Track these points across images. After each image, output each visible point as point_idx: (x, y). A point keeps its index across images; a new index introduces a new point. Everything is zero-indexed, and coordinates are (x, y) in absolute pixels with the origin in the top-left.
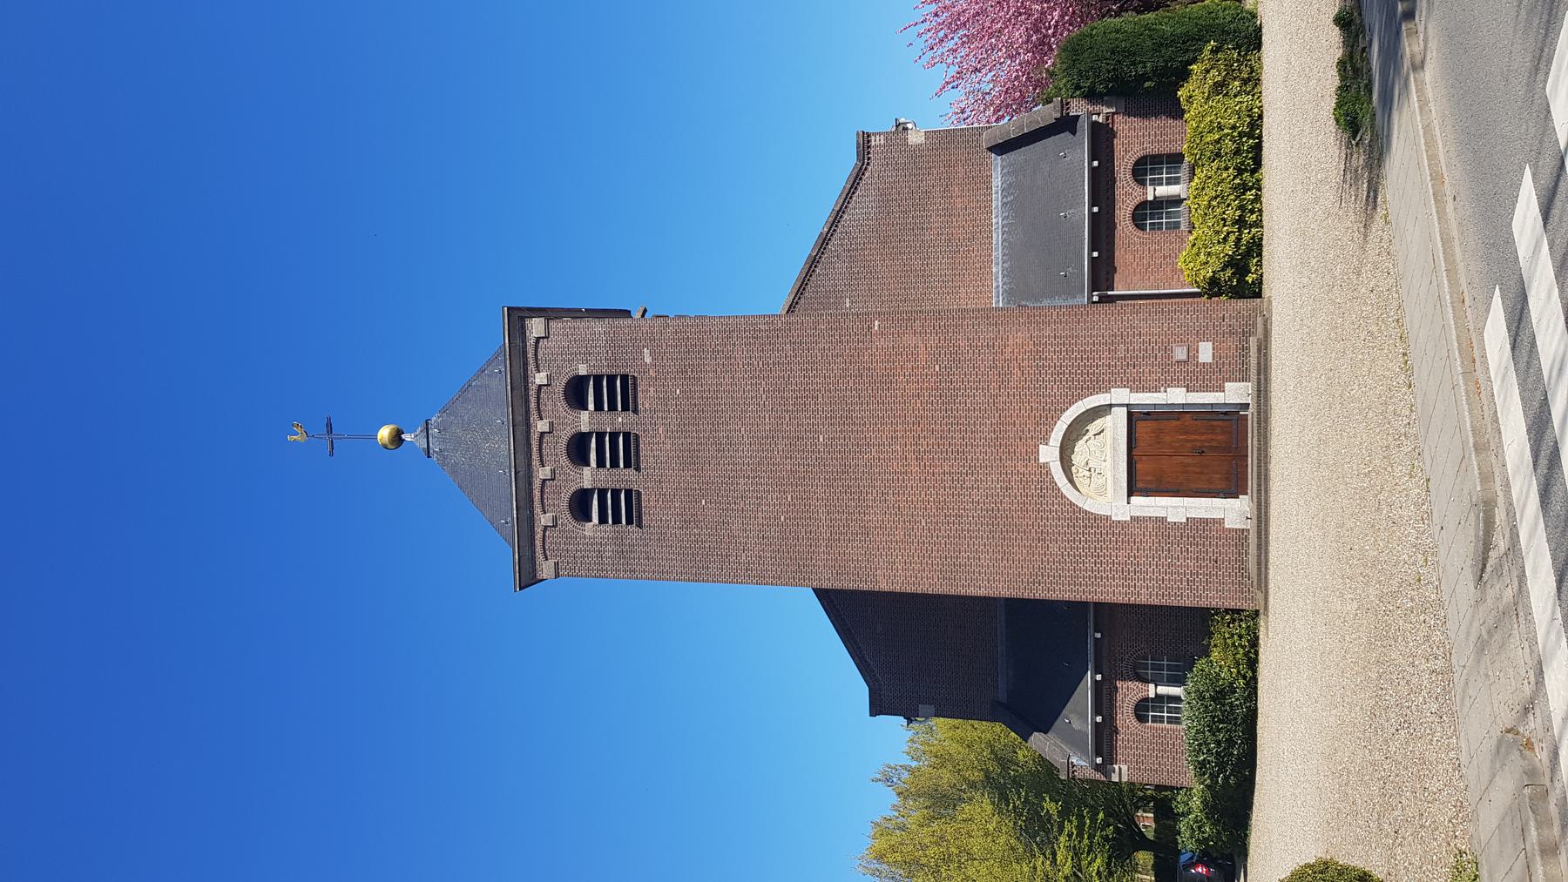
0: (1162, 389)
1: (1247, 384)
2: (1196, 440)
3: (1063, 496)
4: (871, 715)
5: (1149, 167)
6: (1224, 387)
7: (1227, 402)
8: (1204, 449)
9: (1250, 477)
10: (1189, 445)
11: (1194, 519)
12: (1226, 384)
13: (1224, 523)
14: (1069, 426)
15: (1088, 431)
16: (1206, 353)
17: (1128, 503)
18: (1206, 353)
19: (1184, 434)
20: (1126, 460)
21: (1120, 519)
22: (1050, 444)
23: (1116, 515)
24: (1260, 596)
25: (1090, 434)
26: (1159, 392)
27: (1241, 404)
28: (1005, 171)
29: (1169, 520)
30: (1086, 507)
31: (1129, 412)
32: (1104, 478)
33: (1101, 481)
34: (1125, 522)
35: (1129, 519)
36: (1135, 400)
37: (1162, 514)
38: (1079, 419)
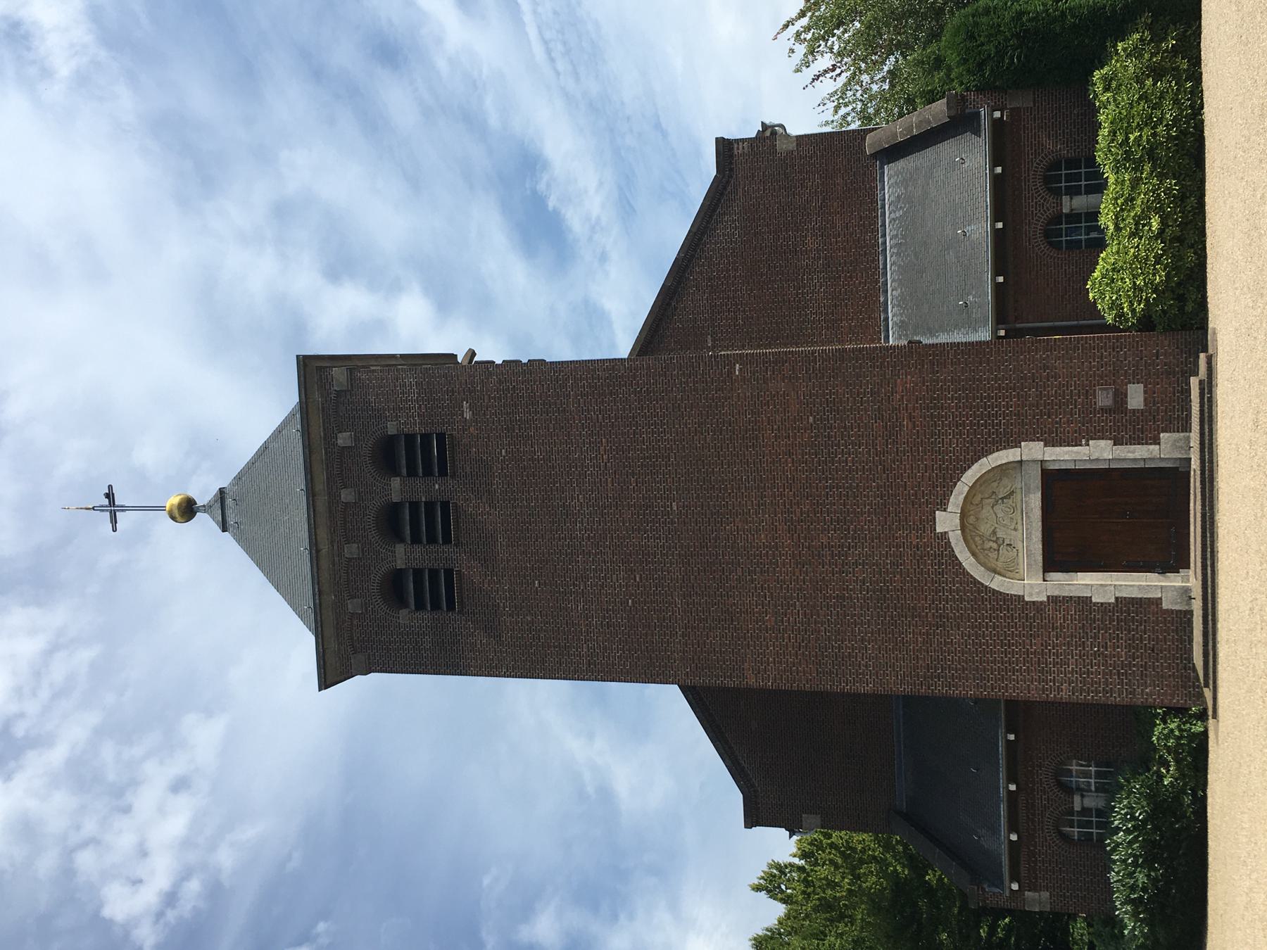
4: (745, 827)
5: (1064, 172)
6: (1159, 439)
9: (1192, 520)
12: (1162, 435)
14: (971, 487)
16: (1136, 397)
18: (1136, 397)
22: (948, 510)
24: (1208, 693)
26: (1081, 445)
27: (1180, 458)
28: (892, 181)
38: (982, 481)
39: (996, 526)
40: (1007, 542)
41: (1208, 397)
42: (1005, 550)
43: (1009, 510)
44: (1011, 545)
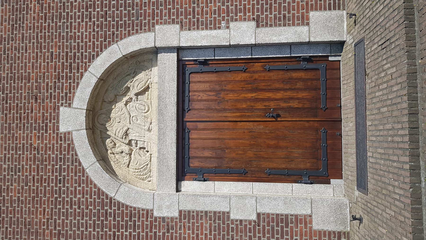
0: (223, 24)
1: (340, 12)
2: (269, 99)
3: (89, 181)
6: (308, 19)
7: (312, 40)
8: (280, 112)
10: (260, 106)
11: (268, 214)
13: (311, 222)
15: (128, 89)
17: (178, 190)
19: (253, 90)
20: (175, 128)
21: (165, 215)
23: (160, 208)
25: (131, 94)
26: (219, 28)
29: (232, 217)
30: (120, 198)
31: (179, 61)
32: (148, 154)
33: (145, 157)
34: (172, 219)
35: (177, 214)
36: (315, 38)
37: (223, 208)
40: (140, 145)
42: (137, 155)
43: (143, 108)
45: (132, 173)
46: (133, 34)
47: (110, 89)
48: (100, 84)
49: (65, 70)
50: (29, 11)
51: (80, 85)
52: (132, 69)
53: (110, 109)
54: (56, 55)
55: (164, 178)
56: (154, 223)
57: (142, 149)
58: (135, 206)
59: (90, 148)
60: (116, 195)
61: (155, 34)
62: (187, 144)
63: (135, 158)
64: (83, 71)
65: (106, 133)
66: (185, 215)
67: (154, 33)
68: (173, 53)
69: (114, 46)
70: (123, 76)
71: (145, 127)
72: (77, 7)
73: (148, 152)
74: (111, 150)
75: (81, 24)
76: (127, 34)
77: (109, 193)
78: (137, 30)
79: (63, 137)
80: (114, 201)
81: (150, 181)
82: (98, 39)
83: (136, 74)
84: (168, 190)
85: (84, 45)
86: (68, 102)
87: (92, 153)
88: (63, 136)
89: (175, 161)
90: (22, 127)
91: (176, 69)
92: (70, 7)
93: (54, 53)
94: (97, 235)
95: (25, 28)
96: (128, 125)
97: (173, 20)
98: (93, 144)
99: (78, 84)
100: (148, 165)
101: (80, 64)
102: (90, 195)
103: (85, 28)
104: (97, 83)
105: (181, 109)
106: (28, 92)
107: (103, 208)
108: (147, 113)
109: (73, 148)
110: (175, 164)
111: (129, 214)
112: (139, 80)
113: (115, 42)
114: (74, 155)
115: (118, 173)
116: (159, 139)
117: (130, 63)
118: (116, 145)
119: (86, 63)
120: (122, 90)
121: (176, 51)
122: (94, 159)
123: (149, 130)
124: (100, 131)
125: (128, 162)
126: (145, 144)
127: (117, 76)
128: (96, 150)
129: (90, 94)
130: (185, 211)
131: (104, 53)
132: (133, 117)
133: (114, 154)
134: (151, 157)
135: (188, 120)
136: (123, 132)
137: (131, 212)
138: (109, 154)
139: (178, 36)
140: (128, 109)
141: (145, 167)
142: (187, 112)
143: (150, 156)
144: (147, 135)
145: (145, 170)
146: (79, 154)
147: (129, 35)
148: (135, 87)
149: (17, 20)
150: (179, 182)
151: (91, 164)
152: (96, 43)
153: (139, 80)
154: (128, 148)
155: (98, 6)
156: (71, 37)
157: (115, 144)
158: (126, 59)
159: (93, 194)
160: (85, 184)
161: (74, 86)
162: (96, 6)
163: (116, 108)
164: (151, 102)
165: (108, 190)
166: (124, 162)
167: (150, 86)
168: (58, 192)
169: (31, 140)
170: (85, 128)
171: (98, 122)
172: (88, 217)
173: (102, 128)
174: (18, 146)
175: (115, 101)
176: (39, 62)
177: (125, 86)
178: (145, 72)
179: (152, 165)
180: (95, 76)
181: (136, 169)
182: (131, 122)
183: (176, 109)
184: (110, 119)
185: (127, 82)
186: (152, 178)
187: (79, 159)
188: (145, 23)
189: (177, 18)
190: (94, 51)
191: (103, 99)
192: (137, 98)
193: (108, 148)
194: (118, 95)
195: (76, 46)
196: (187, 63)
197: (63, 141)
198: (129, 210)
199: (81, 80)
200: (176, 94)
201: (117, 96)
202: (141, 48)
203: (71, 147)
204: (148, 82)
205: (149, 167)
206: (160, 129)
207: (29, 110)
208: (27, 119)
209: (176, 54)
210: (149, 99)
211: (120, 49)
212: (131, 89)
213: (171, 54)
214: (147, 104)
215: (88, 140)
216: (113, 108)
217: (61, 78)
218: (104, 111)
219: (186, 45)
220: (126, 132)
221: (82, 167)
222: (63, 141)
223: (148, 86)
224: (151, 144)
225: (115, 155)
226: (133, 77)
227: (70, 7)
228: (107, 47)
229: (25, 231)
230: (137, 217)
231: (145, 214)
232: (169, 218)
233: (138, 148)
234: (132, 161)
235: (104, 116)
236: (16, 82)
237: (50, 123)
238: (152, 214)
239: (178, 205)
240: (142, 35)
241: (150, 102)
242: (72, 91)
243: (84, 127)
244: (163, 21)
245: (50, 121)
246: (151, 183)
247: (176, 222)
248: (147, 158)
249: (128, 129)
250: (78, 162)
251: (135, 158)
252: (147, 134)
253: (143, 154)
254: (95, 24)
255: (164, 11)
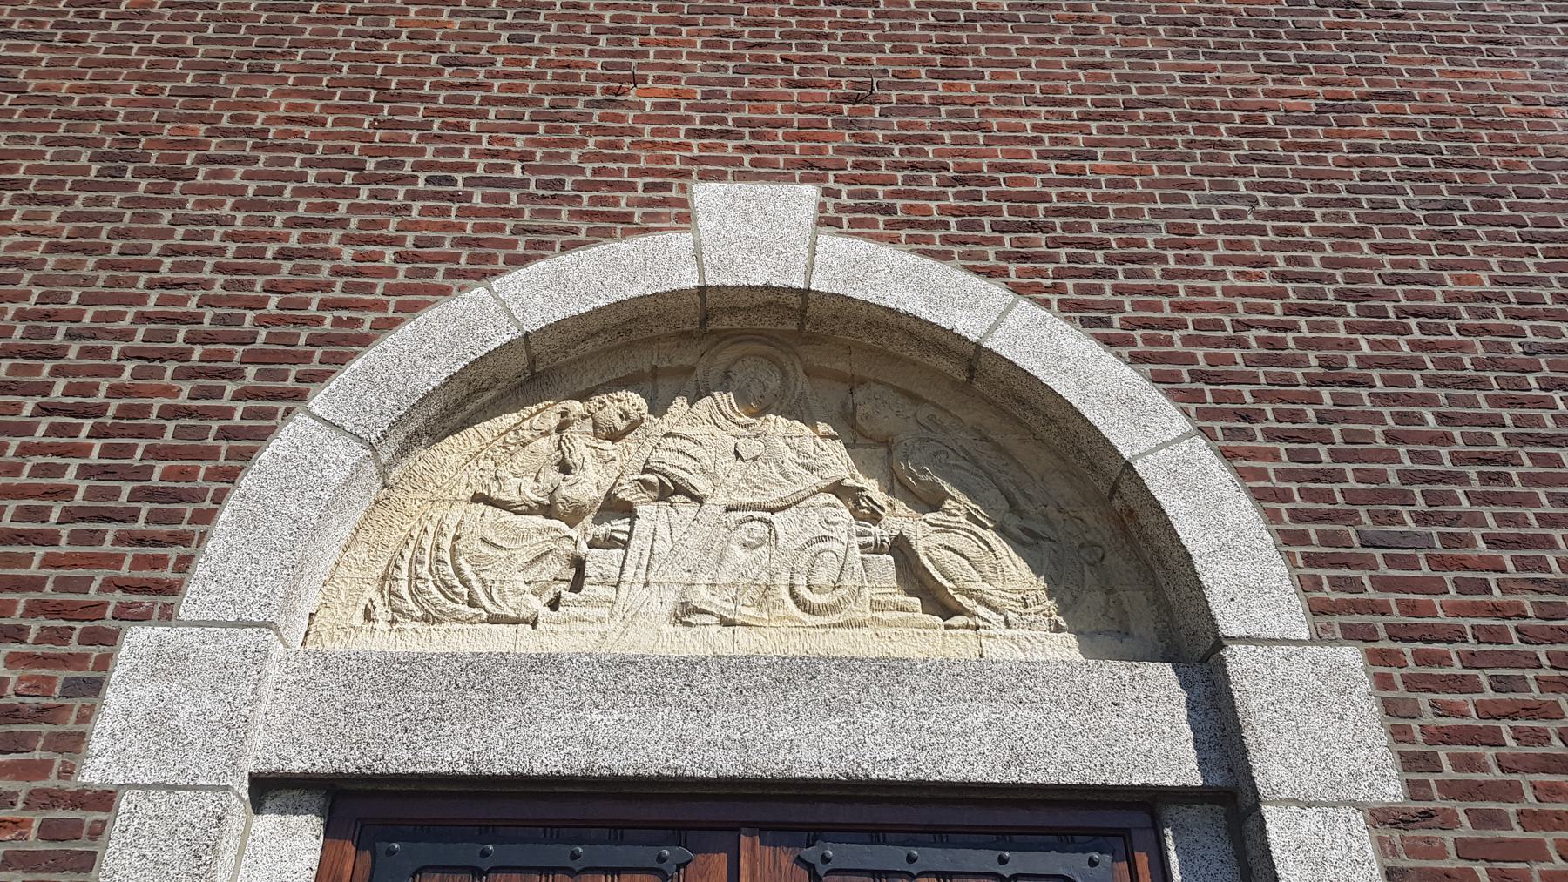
15: (929, 501)
21: (113, 698)
23: (170, 664)
25: (900, 519)
32: (538, 605)
34: (75, 743)
39: (712, 508)
40: (600, 562)
41: (303, 133)
42: (537, 544)
43: (822, 577)
44: (576, 586)
45: (437, 516)
46: (1272, 516)
47: (924, 412)
48: (944, 364)
49: (1009, 204)
50: (1274, 76)
51: (938, 265)
52: (1049, 523)
53: (811, 414)
54: (1081, 172)
55: (366, 698)
56: (79, 626)
57: (571, 574)
58: (223, 517)
59: (602, 303)
60: (310, 421)
61: (1298, 642)
62: (574, 856)
63: (522, 536)
64: (1014, 279)
65: (678, 394)
66: (72, 830)
67: (1305, 635)
68: (1202, 763)
69: (1173, 420)
70: (1003, 477)
71: (702, 590)
72: (1351, 255)
73: (554, 605)
74: (584, 417)
75: (1267, 272)
76: (1262, 484)
77: (333, 386)
78: (1302, 538)
79: (667, 194)
80: (281, 413)
81: (368, 615)
82: (1203, 345)
83: (1023, 544)
84: (278, 722)
85: (1155, 283)
86: (845, 218)
87: (574, 312)
88: (674, 194)
89: (464, 769)
90: (719, 51)
91: (1094, 778)
92: (1341, 225)
93: (1087, 164)
94: (110, 332)
95: (1190, 62)
96: (723, 500)
97: (1431, 763)
98: (623, 329)
99: (944, 256)
100: (472, 603)
101: (1050, 267)
102: (341, 300)
103: (1250, 288)
104: (952, 343)
105: (823, 813)
106: (885, 71)
107: (251, 358)
108: (790, 602)
109: (608, 234)
110: (445, 769)
111: (182, 485)
112: (986, 560)
113: (1201, 424)
114: (572, 237)
115: (447, 448)
116: (621, 665)
117: (1084, 514)
118: (613, 441)
119: (1054, 289)
120: (924, 472)
121: (1217, 780)
122: (534, 321)
123: (686, 613)
124: (692, 369)
125: (503, 496)
126: (602, 591)
127: (999, 448)
128: (590, 346)
129: (893, 306)
130: (97, 831)
131: (1128, 370)
132: (769, 523)
133: (560, 429)
134: (516, 622)
135: (744, 864)
136: (682, 474)
137: (194, 496)
138: (559, 407)
139: (1330, 794)
140: (811, 500)
141: (461, 589)
142: (799, 860)
143: (525, 614)
144: (655, 602)
145: (445, 588)
146: (569, 258)
147: (1259, 496)
148: (943, 539)
149: (1222, 36)
150: (318, 800)
151: (514, 307)
152: (1176, 335)
153: (986, 560)
154: (585, 500)
155: (1386, 345)
156: (1186, 231)
157: (614, 436)
158: (1106, 490)
159: (345, 314)
160: (407, 281)
161: (929, 241)
162: (1380, 337)
163: (818, 440)
164: (861, 625)
165: (349, 380)
166: (507, 474)
167: (957, 620)
168: (387, 172)
169: (658, 79)
170: (709, 283)
171: (736, 361)
172: (224, 293)
173: (706, 374)
174: (632, 37)
175: (855, 435)
176: (1034, 108)
177: (947, 487)
178: (1041, 592)
179: (465, 626)
180: (993, 327)
181: (456, 538)
182: (740, 515)
183: (817, 773)
184: (756, 415)
185: (973, 497)
186: (387, 627)
187: (543, 257)
188: (1356, 585)
189: (1451, 790)
190: (1130, 324)
191: (862, 382)
192: (878, 549)
193: (595, 400)
194: (890, 453)
195: (1142, 250)
196: (1142, 860)
197: (646, 195)
198: (205, 485)
199: (964, 267)
200: (922, 776)
201: (882, 451)
202: (1196, 559)
203: (612, 225)
204: (981, 610)
205: (453, 611)
206: (688, 667)
207: (799, 74)
208: (760, 68)
209: (1196, 780)
210: (880, 615)
211: (1165, 445)
212: (929, 516)
213: (1191, 746)
214: (847, 602)
215: (644, 296)
216: (814, 427)
217: (967, 188)
218: (802, 384)
219: (1276, 853)
220: (680, 489)
221: (501, 271)
222: (646, 195)
223: (961, 611)
224: (601, 620)
225: (555, 437)
226: (1001, 530)
227: (1341, 225)
228: (1161, 386)
229: (226, 55)
230: (153, 528)
231: (157, 574)
232: (84, 718)
233: (583, 548)
234: (507, 516)
235: (774, 383)
236: (933, 34)
237: (736, 148)
238: (143, 618)
239: (156, 786)
240: (1279, 568)
241: (859, 616)
242: (903, 233)
243: (713, 280)
244: (1401, 692)
245: (747, 148)
246: (358, 619)
247: (43, 768)
248: (512, 600)
249: (699, 500)
250: (532, 252)
251: (522, 536)
252: (663, 602)
253: (545, 576)
254: (1278, 329)
255: (1467, 700)
